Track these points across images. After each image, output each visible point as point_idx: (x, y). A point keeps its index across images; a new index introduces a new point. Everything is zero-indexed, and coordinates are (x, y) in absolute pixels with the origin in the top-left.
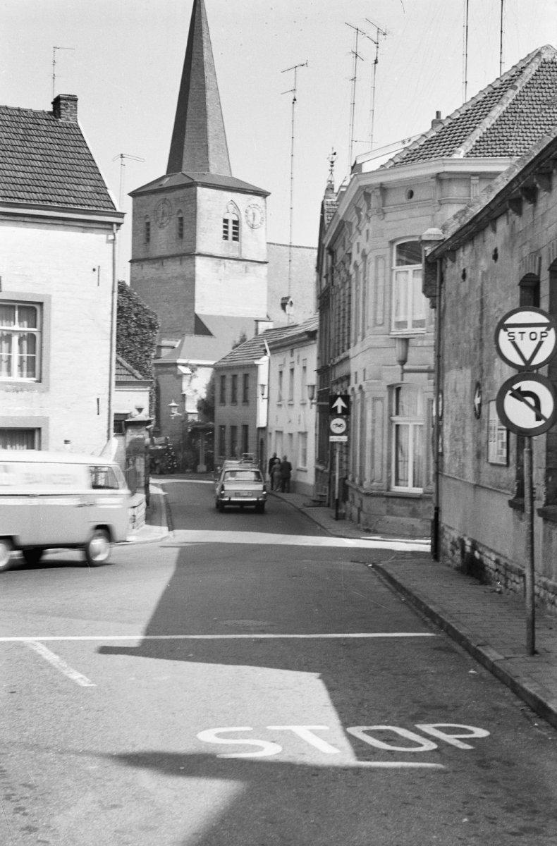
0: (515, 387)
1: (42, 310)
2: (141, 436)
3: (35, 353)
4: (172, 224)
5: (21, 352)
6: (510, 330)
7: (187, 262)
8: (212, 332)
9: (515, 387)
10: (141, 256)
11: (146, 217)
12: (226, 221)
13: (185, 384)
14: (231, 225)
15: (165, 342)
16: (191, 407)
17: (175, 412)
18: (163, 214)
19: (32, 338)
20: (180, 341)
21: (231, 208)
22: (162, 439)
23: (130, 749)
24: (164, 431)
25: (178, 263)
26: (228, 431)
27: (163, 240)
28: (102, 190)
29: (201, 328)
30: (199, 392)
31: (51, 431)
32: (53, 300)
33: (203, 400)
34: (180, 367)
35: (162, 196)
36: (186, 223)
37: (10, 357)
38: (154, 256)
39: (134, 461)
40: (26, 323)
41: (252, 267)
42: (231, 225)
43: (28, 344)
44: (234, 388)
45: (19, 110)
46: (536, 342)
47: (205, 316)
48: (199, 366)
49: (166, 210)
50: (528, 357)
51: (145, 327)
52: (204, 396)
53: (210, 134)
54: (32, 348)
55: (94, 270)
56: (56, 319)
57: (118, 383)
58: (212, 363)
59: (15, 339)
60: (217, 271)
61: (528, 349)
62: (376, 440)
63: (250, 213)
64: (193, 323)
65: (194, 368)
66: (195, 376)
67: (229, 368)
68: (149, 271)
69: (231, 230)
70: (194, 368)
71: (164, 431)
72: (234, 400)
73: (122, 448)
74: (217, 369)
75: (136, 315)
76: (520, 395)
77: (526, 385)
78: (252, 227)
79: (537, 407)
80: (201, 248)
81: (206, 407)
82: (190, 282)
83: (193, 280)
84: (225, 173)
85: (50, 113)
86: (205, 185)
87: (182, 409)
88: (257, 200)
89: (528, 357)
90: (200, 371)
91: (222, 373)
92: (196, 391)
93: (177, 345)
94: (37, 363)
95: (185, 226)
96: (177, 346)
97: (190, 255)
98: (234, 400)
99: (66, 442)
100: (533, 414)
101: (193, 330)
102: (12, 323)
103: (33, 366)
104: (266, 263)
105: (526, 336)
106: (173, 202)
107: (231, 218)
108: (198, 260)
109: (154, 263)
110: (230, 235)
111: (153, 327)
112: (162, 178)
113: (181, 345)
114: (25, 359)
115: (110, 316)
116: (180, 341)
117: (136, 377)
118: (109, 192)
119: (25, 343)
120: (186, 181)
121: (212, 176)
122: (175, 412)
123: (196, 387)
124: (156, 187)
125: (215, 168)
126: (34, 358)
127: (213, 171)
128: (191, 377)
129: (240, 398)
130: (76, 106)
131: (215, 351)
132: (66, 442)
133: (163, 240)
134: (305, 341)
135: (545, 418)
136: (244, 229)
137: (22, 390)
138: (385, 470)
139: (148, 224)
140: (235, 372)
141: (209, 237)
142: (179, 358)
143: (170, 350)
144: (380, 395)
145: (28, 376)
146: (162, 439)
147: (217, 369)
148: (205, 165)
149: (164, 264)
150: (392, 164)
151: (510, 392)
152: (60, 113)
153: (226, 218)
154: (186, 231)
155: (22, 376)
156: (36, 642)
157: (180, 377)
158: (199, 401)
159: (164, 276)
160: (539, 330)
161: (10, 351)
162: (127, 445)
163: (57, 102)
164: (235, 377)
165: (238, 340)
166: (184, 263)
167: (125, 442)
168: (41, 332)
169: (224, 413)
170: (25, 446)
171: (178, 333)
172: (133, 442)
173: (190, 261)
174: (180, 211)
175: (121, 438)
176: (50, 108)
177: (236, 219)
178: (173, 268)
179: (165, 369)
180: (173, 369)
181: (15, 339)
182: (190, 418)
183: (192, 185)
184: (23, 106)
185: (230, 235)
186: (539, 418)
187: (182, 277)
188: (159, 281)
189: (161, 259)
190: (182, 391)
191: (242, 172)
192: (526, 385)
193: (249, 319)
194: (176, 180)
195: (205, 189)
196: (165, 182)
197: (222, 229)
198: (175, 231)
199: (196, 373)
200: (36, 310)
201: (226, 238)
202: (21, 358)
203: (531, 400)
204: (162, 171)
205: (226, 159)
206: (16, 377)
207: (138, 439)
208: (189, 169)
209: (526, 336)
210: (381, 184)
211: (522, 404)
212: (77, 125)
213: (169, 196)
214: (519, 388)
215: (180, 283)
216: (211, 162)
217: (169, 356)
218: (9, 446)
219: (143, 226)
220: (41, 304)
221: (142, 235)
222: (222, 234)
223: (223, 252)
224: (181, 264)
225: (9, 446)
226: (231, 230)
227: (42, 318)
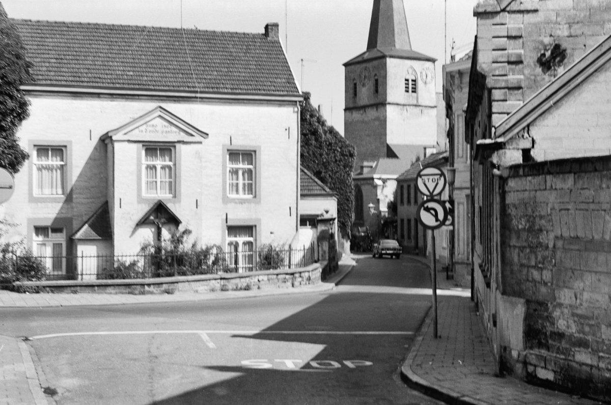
0: (426, 205)
1: (255, 154)
2: (326, 228)
3: (252, 180)
4: (370, 84)
5: (244, 179)
6: (423, 177)
7: (381, 109)
8: (398, 155)
9: (426, 205)
10: (351, 105)
11: (354, 79)
12: (407, 80)
13: (379, 191)
14: (410, 83)
15: (365, 164)
16: (384, 208)
17: (373, 211)
18: (365, 77)
19: (250, 171)
20: (376, 163)
21: (410, 71)
22: (364, 229)
23: (209, 365)
24: (365, 223)
25: (375, 110)
26: (406, 222)
27: (365, 94)
28: (292, 81)
29: (391, 154)
30: (389, 197)
31: (262, 227)
32: (262, 149)
33: (391, 202)
34: (375, 180)
35: (364, 65)
36: (380, 83)
37: (237, 184)
38: (359, 106)
39: (322, 244)
40: (246, 163)
41: (426, 111)
42: (410, 83)
43: (248, 176)
44: (409, 194)
45: (244, 34)
46: (435, 183)
47: (395, 145)
48: (389, 179)
49: (367, 75)
50: (431, 191)
51: (347, 156)
52: (392, 199)
53: (395, 21)
54: (250, 178)
55: (286, 130)
56: (263, 158)
57: (303, 196)
58: (395, 177)
59: (240, 173)
60: (401, 114)
61: (431, 186)
62: (460, 229)
63: (424, 74)
64: (385, 149)
65: (384, 181)
66: (385, 186)
67: (405, 181)
68: (356, 115)
69: (410, 86)
70: (384, 181)
71: (366, 223)
72: (409, 202)
73: (315, 236)
74: (398, 180)
75: (341, 148)
76: (428, 210)
77: (431, 205)
78: (425, 83)
79: (436, 216)
80: (390, 99)
81: (393, 207)
82: (383, 122)
83: (385, 121)
84: (407, 48)
85: (263, 34)
86: (391, 57)
87: (377, 208)
88: (429, 64)
89: (431, 191)
90: (389, 183)
91: (401, 184)
92: (386, 196)
93: (374, 165)
94: (253, 187)
95: (379, 85)
96: (374, 166)
97: (381, 104)
98: (409, 202)
99: (271, 233)
100: (434, 219)
101: (386, 154)
102: (238, 163)
103: (250, 189)
104: (436, 107)
105: (430, 180)
106: (371, 69)
107: (411, 77)
108: (388, 106)
109: (360, 110)
110: (410, 90)
111: (352, 155)
112: (364, 53)
113: (377, 165)
114: (247, 184)
115: (296, 157)
116: (376, 163)
117: (325, 191)
118: (296, 82)
119: (246, 175)
120: (380, 54)
121: (398, 51)
122: (373, 211)
123: (386, 194)
124: (360, 59)
125: (400, 44)
126: (252, 184)
127: (398, 46)
128: (383, 187)
129: (412, 200)
130: (278, 29)
131: (402, 166)
132: (271, 233)
133: (365, 94)
134: (443, 163)
135: (440, 221)
136: (420, 84)
137: (245, 203)
138: (466, 247)
139: (355, 84)
140: (409, 183)
141: (395, 91)
142: (374, 173)
143: (369, 169)
144: (462, 201)
145: (248, 194)
146: (364, 229)
147: (398, 181)
148: (392, 43)
149: (366, 110)
150: (467, 57)
151: (422, 208)
152: (268, 34)
153: (407, 78)
154: (380, 89)
155: (245, 194)
156: (204, 334)
157: (375, 187)
158: (388, 204)
159: (366, 119)
160: (436, 177)
161: (237, 179)
162: (318, 234)
163: (267, 27)
164: (409, 186)
165: (414, 160)
166: (379, 110)
167: (317, 232)
168: (255, 168)
169: (405, 211)
170: (248, 236)
171: (374, 157)
172: (323, 232)
173: (382, 108)
174: (376, 75)
175: (315, 230)
176: (263, 32)
177: (414, 78)
178: (372, 113)
179: (365, 182)
180: (371, 181)
181: (240, 173)
182: (383, 214)
183: (384, 57)
184: (247, 31)
185: (410, 90)
186: (437, 220)
187: (377, 119)
188: (363, 122)
189: (364, 107)
190: (377, 196)
191: (418, 47)
192: (431, 205)
193: (419, 146)
194: (374, 53)
195: (392, 59)
196: (366, 56)
197: (404, 86)
198: (373, 89)
199: (386, 184)
200: (252, 155)
201: (407, 91)
202: (244, 184)
203: (433, 212)
204: (364, 49)
205: (407, 38)
206: (242, 195)
207: (325, 230)
208: (381, 47)
209: (430, 180)
210: (459, 71)
211: (429, 214)
212: (279, 41)
213: (369, 65)
214: (427, 207)
215: (377, 123)
216: (396, 40)
217: (369, 173)
218: (238, 236)
219: (352, 86)
220: (255, 151)
221: (352, 91)
222: (404, 89)
223: (406, 102)
224: (377, 110)
225: (238, 236)
226: (410, 86)
227: (256, 159)
